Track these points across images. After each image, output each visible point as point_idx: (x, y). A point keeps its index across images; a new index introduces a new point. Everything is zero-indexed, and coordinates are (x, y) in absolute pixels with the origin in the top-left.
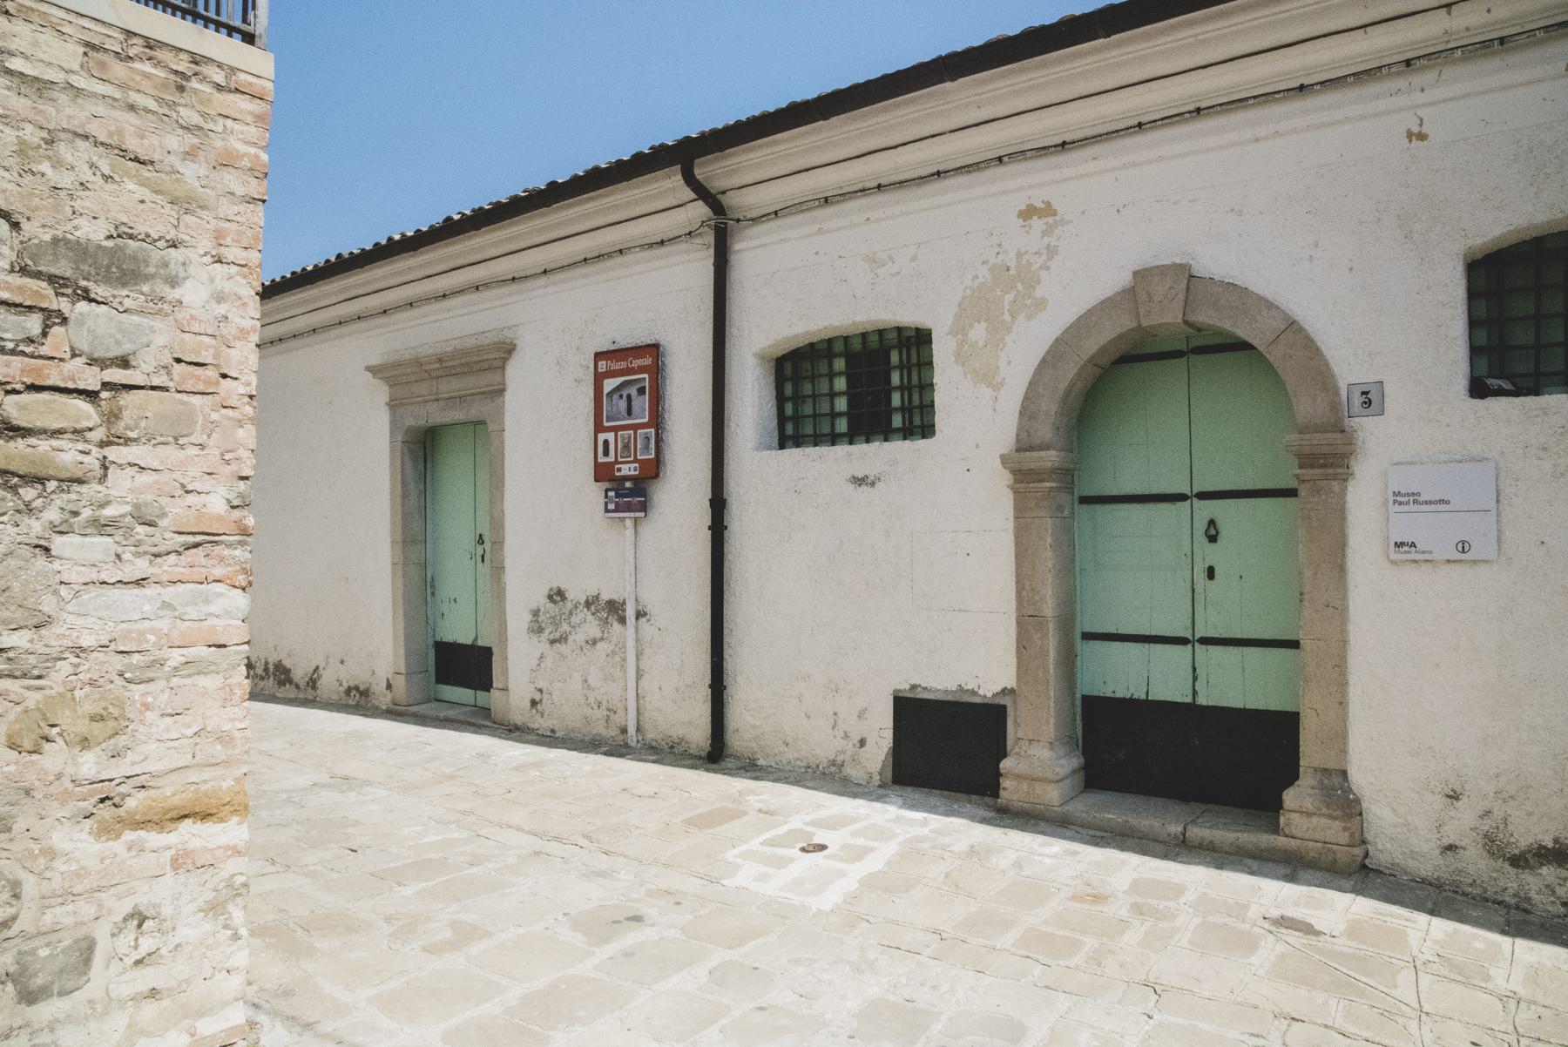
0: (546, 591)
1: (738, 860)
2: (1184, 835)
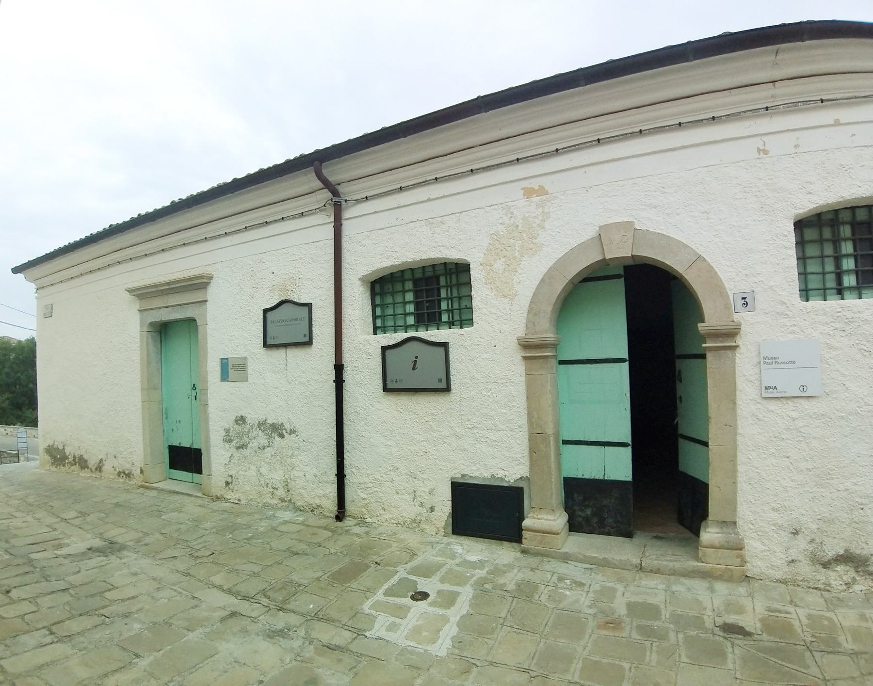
0: (234, 418)
1: (373, 612)
2: (641, 565)
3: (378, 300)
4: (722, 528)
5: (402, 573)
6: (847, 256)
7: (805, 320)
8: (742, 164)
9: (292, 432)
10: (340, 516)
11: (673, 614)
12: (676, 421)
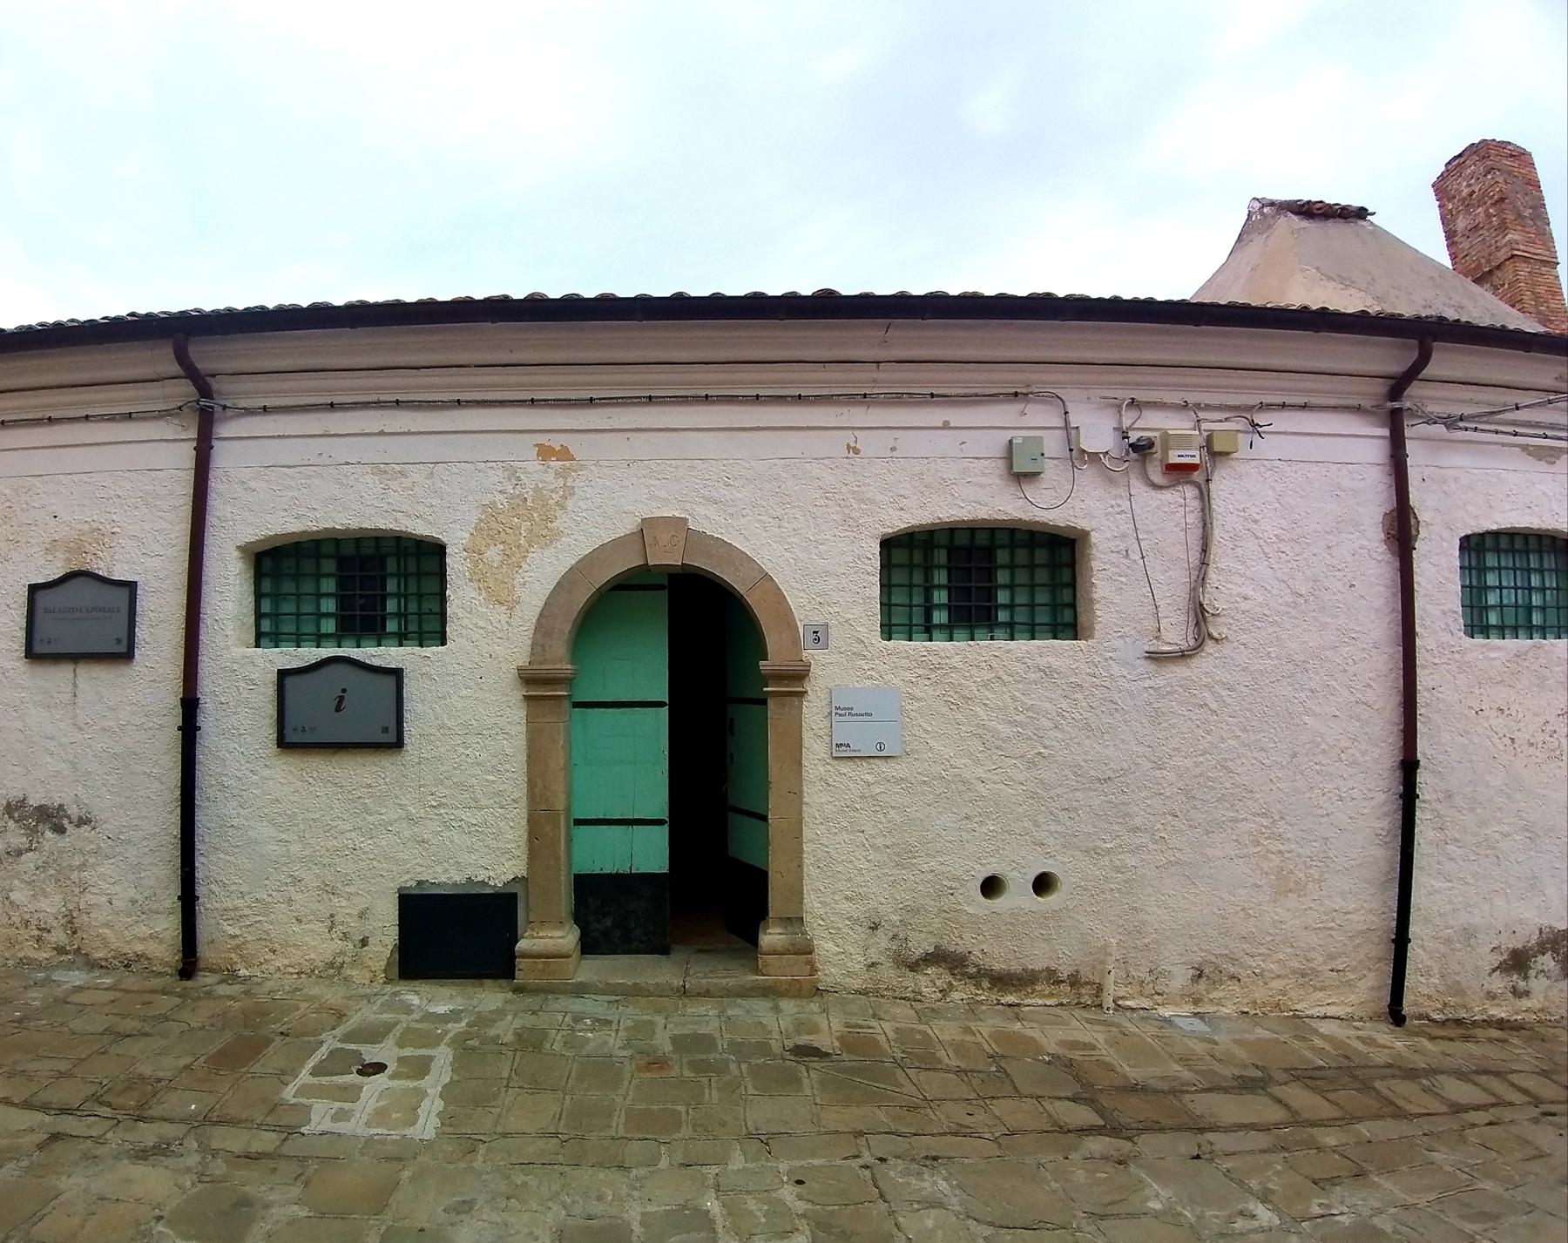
3: (267, 586)
4: (785, 927)
5: (330, 1042)
6: (939, 587)
7: (885, 663)
8: (826, 462)
9: (82, 822)
10: (189, 964)
11: (731, 1043)
12: (724, 788)
